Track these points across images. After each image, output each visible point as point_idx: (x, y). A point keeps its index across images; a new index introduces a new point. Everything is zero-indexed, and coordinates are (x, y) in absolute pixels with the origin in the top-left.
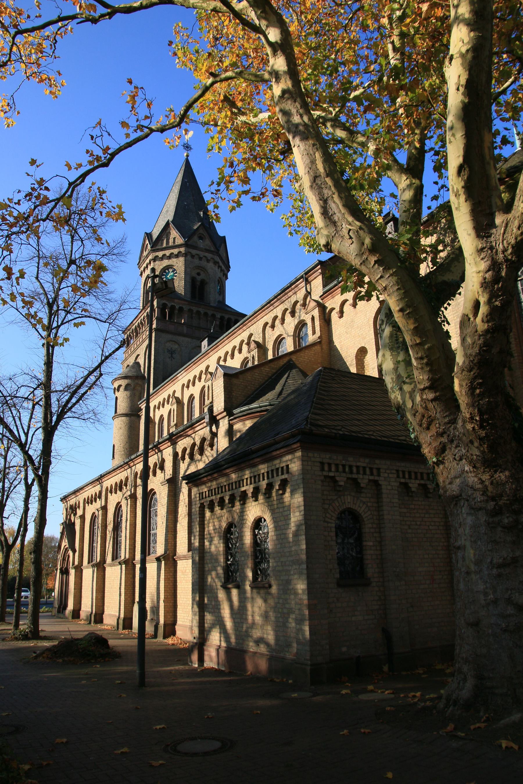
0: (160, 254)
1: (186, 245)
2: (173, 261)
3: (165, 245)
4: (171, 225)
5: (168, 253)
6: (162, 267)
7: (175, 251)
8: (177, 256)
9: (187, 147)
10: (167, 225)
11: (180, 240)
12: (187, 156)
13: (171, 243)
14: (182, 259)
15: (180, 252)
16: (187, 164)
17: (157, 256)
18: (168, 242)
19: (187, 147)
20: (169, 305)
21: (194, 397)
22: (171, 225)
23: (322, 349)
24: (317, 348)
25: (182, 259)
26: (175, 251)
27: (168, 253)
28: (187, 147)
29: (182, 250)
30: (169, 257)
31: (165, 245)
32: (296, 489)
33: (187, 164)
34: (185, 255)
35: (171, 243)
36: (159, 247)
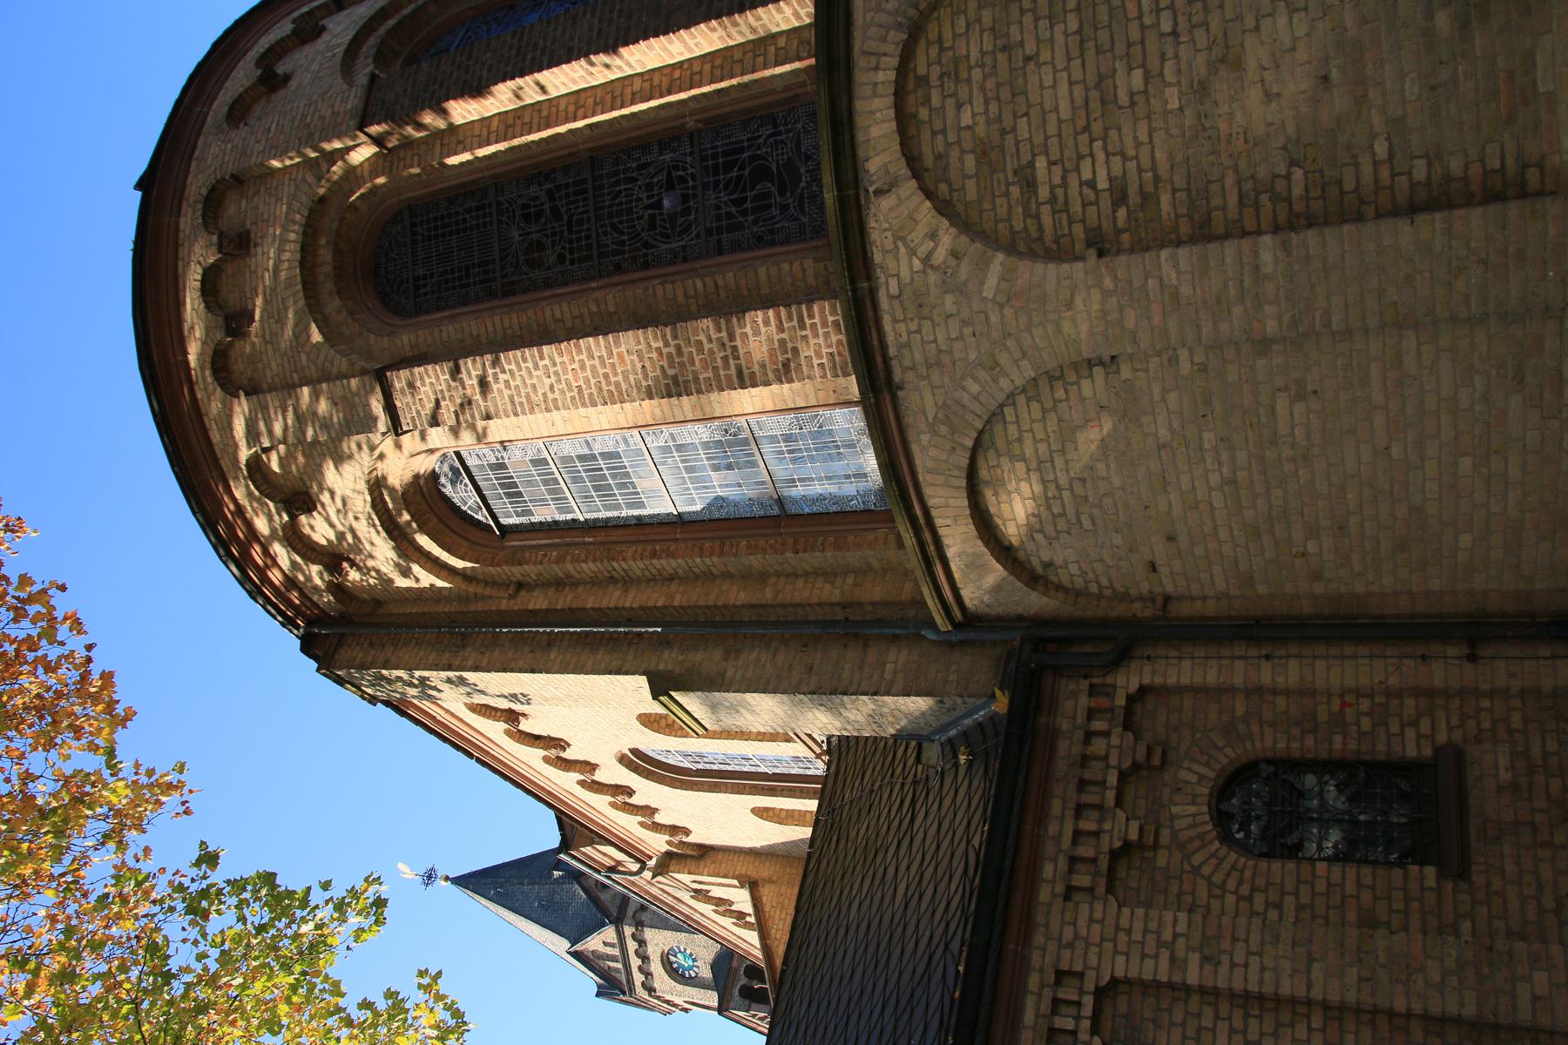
0: (638, 978)
1: (618, 922)
2: (654, 952)
3: (619, 966)
4: (578, 947)
5: (635, 962)
6: (666, 977)
7: (632, 946)
8: (642, 943)
9: (429, 877)
10: (577, 955)
11: (609, 933)
12: (447, 878)
13: (616, 952)
14: (649, 934)
15: (634, 936)
16: (480, 882)
17: (643, 984)
18: (613, 959)
19: (429, 877)
20: (743, 980)
21: (635, 751)
22: (578, 947)
23: (770, 881)
24: (767, 893)
25: (649, 934)
26: (632, 946)
27: (635, 962)
28: (430, 877)
29: (628, 931)
30: (645, 958)
31: (619, 966)
32: (594, 892)
33: (480, 882)
34: (639, 924)
35: (616, 952)
36: (623, 979)
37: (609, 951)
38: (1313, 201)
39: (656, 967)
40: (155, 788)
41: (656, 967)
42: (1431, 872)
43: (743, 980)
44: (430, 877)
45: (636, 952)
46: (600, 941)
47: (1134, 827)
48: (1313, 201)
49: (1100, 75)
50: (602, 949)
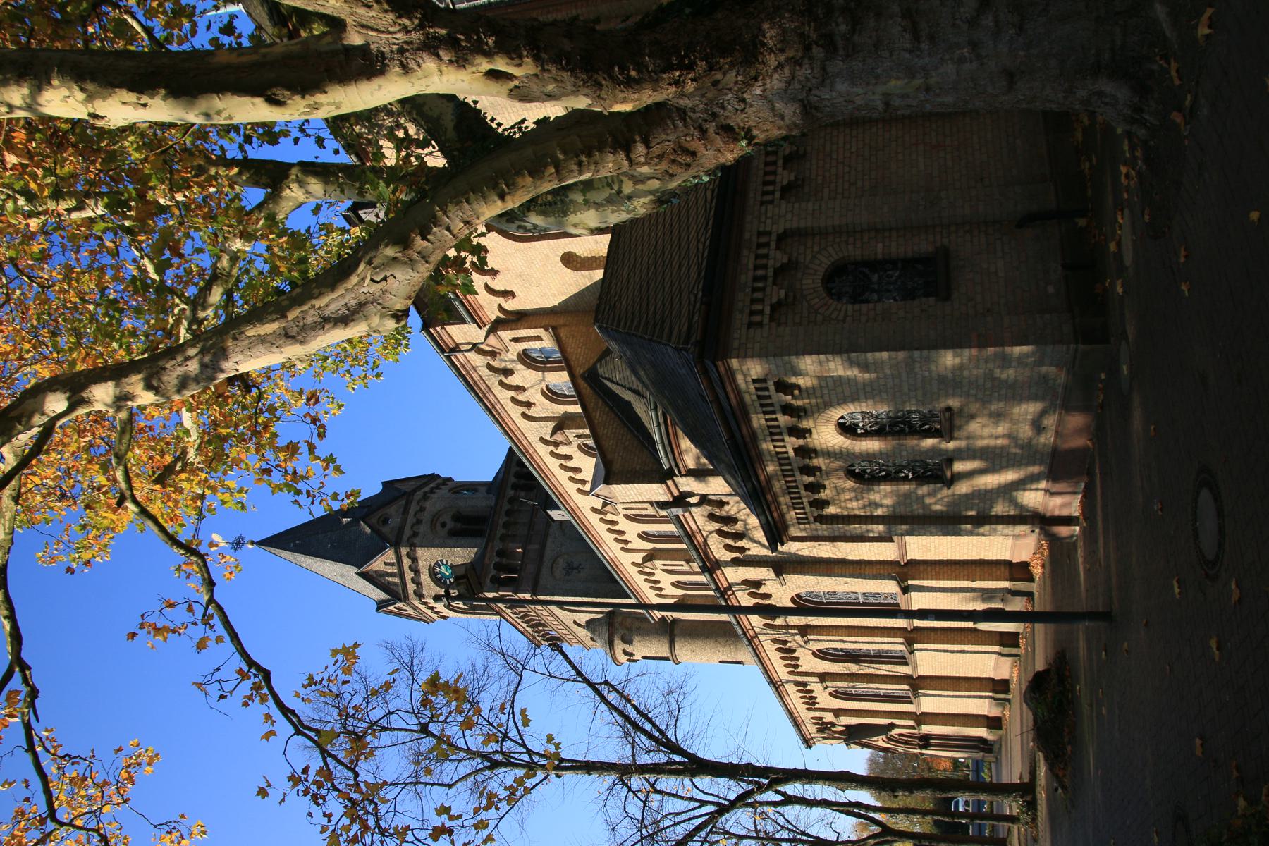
0: (411, 587)
1: (396, 545)
2: (423, 566)
3: (397, 580)
4: (365, 569)
5: (409, 575)
6: (432, 585)
7: (406, 562)
8: (414, 560)
9: (238, 543)
10: (364, 575)
11: (389, 555)
12: (252, 543)
13: (394, 570)
14: (420, 552)
17: (415, 592)
18: (392, 575)
19: (238, 543)
20: (493, 572)
22: (365, 569)
25: (420, 552)
26: (406, 562)
27: (409, 575)
28: (238, 543)
29: (404, 551)
30: (417, 572)
31: (397, 580)
34: (413, 546)
35: (394, 570)
37: (390, 569)
38: (1028, 220)
39: (425, 578)
40: (308, 230)
41: (425, 578)
42: (932, 300)
43: (493, 572)
44: (238, 543)
45: (410, 567)
46: (382, 562)
47: (782, 293)
48: (1028, 220)
49: (456, 349)
50: (383, 568)
